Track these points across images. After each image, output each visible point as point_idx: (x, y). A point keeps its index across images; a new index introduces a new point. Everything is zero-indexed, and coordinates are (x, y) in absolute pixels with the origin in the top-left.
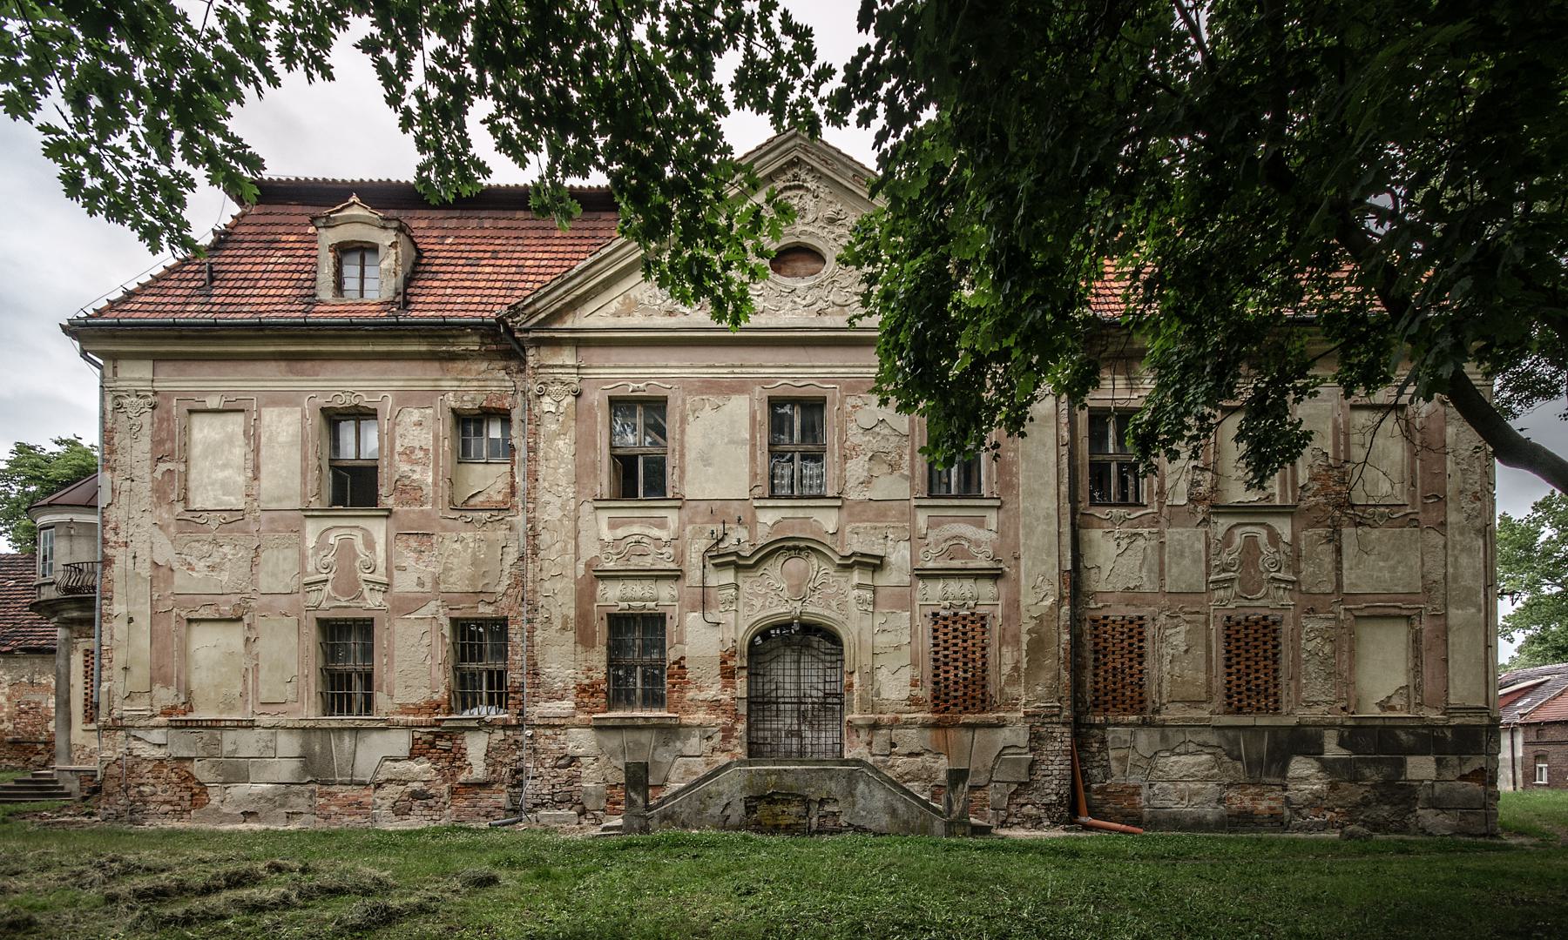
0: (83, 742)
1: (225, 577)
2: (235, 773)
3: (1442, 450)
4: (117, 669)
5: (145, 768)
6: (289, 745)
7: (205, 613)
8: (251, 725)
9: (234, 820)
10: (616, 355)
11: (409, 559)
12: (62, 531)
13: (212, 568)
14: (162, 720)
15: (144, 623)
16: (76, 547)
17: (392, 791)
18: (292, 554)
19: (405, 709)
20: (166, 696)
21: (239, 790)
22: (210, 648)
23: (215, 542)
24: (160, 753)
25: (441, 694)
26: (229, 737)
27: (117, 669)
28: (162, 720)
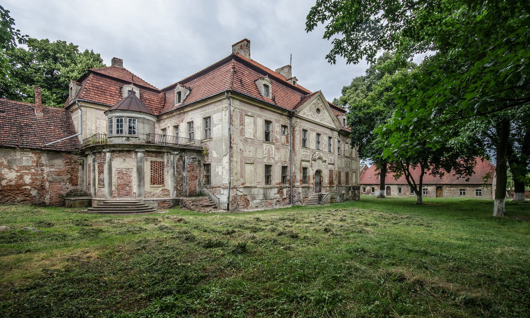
0: (150, 191)
1: (251, 154)
2: (254, 198)
3: (135, 93)
4: (234, 174)
5: (238, 198)
6: (261, 191)
7: (248, 162)
8: (255, 187)
9: (253, 208)
10: (307, 123)
11: (277, 154)
12: (141, 121)
13: (249, 151)
14: (242, 186)
15: (239, 163)
16: (145, 126)
17: (275, 200)
18: (262, 150)
19: (277, 184)
20: (242, 181)
21: (255, 201)
22: (249, 168)
23: (250, 146)
24: (241, 194)
25: (280, 181)
26: (253, 190)
27: (234, 174)
28: (242, 186)
